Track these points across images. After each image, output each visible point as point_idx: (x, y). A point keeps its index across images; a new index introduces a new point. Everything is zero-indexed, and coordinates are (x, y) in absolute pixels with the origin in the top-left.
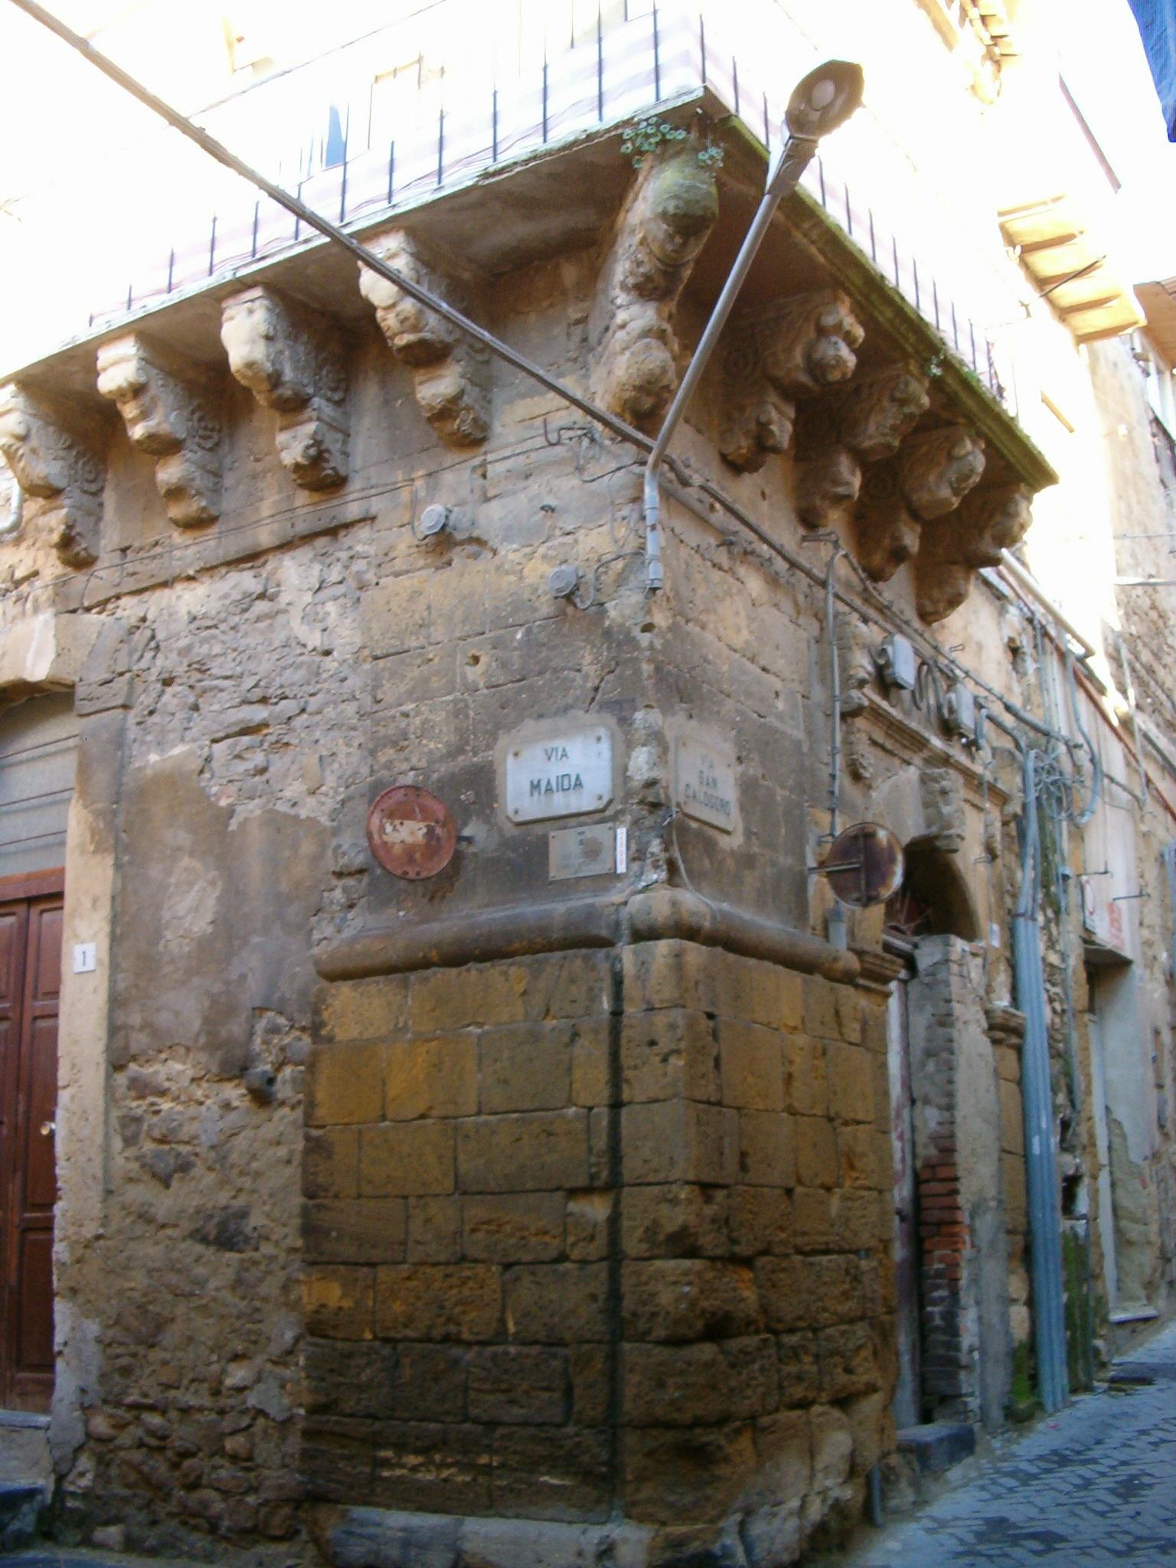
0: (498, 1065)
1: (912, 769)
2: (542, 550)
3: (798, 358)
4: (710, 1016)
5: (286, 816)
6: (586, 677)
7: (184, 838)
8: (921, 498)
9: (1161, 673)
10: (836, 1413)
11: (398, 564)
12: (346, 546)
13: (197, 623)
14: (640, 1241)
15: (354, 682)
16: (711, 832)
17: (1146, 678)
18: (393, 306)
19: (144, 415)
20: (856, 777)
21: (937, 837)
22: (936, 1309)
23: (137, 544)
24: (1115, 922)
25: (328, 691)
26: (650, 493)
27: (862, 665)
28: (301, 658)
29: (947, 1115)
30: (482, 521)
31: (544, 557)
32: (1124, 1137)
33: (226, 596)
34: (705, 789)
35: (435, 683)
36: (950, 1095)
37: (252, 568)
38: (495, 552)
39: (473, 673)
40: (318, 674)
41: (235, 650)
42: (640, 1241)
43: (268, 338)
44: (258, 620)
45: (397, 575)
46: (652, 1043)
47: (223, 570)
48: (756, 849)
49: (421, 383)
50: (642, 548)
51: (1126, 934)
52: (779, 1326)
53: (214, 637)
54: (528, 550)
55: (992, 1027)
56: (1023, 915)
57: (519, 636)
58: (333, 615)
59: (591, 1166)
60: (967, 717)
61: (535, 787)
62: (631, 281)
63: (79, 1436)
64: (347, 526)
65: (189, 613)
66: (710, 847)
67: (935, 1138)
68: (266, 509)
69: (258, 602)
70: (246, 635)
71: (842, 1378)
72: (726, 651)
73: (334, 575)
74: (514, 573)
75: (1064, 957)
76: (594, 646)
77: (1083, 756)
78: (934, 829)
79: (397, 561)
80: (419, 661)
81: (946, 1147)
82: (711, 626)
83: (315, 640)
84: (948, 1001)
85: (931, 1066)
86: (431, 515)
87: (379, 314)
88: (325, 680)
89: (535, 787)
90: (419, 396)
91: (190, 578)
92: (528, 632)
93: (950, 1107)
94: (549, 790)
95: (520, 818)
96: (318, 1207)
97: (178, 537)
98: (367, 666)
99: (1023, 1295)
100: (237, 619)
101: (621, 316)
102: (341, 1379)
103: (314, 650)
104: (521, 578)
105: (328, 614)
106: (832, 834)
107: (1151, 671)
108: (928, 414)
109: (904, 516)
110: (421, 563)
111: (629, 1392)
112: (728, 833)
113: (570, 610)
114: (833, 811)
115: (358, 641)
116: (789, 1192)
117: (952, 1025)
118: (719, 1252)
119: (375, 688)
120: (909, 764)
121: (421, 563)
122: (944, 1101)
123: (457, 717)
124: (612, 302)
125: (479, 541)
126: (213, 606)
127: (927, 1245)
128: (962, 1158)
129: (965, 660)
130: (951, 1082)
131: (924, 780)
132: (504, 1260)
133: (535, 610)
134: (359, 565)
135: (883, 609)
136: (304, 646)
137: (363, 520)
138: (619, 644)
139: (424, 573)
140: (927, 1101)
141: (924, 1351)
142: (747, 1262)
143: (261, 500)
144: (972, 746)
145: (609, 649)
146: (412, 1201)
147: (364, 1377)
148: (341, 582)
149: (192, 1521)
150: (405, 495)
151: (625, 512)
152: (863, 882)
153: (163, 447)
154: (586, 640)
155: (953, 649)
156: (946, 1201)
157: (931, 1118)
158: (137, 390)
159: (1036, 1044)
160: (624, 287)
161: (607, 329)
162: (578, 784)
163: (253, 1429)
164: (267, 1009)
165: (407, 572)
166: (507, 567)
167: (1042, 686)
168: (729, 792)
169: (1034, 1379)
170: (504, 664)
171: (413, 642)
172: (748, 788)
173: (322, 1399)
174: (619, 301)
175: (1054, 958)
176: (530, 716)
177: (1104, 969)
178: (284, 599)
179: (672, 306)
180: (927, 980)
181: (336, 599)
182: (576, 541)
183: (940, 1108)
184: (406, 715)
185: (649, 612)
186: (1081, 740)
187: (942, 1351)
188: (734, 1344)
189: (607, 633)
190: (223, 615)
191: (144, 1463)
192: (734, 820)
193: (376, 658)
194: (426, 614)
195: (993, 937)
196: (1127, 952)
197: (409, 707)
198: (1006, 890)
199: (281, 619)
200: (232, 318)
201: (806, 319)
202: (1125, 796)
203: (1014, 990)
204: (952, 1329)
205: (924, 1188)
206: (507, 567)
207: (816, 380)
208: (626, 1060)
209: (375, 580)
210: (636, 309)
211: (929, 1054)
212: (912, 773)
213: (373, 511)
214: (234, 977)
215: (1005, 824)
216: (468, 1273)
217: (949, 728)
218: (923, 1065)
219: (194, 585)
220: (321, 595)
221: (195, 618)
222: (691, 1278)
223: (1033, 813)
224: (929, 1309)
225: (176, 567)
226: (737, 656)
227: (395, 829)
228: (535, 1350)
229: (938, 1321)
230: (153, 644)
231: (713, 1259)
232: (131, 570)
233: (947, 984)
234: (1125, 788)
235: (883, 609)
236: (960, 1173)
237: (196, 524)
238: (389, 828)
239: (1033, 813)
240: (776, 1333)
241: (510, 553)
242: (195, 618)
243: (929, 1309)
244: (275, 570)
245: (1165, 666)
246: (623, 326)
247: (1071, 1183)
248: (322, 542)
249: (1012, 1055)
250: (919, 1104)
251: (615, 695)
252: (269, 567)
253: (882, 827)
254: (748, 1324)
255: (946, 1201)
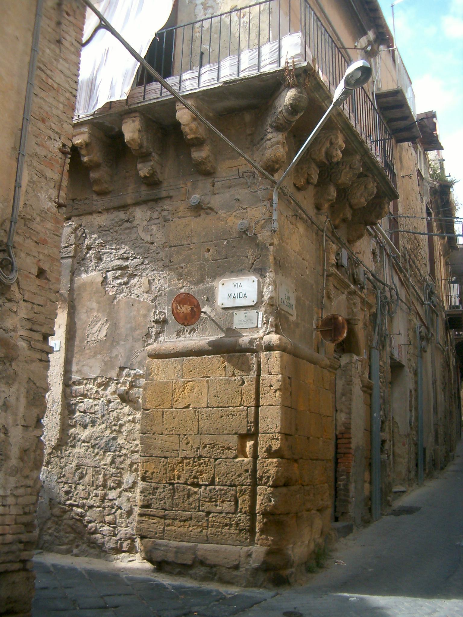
0: (215, 391)
1: (344, 295)
2: (234, 214)
3: (323, 150)
4: (289, 378)
5: (135, 300)
6: (249, 260)
7: (95, 305)
8: (354, 201)
9: (417, 262)
10: (318, 513)
11: (180, 214)
12: (160, 205)
13: (101, 229)
14: (265, 452)
15: (162, 254)
16: (287, 315)
17: (413, 264)
18: (188, 124)
19: (88, 154)
20: (329, 297)
21: (351, 319)
22: (342, 483)
23: (78, 198)
24: (400, 352)
25: (152, 257)
26: (275, 198)
27: (333, 259)
28: (142, 245)
29: (348, 415)
30: (212, 202)
31: (235, 216)
32: (398, 427)
33: (113, 220)
34: (286, 300)
35: (193, 257)
36: (350, 409)
37: (123, 210)
38: (217, 213)
39: (207, 255)
40: (148, 250)
41: (116, 239)
42: (265, 452)
43: (139, 131)
44: (126, 229)
45: (179, 218)
46: (271, 386)
47: (112, 210)
48: (299, 322)
49: (194, 152)
50: (271, 216)
51: (403, 357)
52: (304, 484)
53: (108, 234)
54: (228, 213)
55: (363, 386)
56: (374, 348)
57: (225, 243)
58: (154, 230)
59: (248, 427)
60: (362, 278)
61: (229, 296)
62: (274, 124)
63: (48, 514)
64: (161, 199)
65: (99, 225)
66: (287, 319)
67: (344, 424)
68: (130, 190)
69: (125, 223)
70: (120, 234)
71: (321, 503)
72: (293, 253)
73: (155, 215)
74: (223, 221)
75: (384, 363)
76: (252, 249)
77: (394, 293)
78: (350, 317)
79: (180, 213)
80: (187, 249)
81: (348, 427)
82: (289, 244)
83: (148, 238)
84: (351, 376)
85: (344, 399)
86: (195, 198)
87: (182, 127)
88: (151, 253)
89: (229, 296)
90: (193, 156)
91: (99, 212)
92: (228, 242)
93: (350, 413)
94: (234, 297)
95: (224, 306)
96: (147, 437)
97: (95, 197)
98: (167, 249)
99: (368, 480)
100: (117, 228)
101: (269, 136)
102: (154, 497)
103: (147, 241)
104: (226, 223)
105: (153, 229)
106: (322, 318)
107: (414, 262)
108: (362, 173)
109: (347, 205)
110: (189, 214)
111: (258, 502)
112: (292, 315)
113: (244, 236)
114: (322, 309)
115: (164, 240)
116: (308, 438)
117: (352, 385)
118: (289, 457)
119: (170, 257)
120: (343, 293)
121: (189, 214)
122: (347, 411)
123: (201, 270)
124: (266, 130)
125: (211, 209)
126: (107, 223)
127: (339, 461)
128: (353, 431)
129: (360, 257)
130: (350, 405)
131: (348, 300)
132: (216, 457)
133: (231, 235)
134: (165, 213)
135: (338, 239)
136: (144, 240)
137: (167, 197)
138: (262, 249)
139: (190, 218)
140: (341, 411)
141: (336, 497)
142: (296, 461)
143: (128, 186)
144: (362, 288)
145: (258, 250)
146: (182, 436)
147: (161, 496)
148: (158, 219)
149: (92, 545)
150: (183, 190)
151: (265, 203)
152: (333, 335)
153: (96, 166)
154: (250, 247)
155: (356, 253)
156: (347, 446)
157: (342, 417)
158: (87, 145)
159: (376, 392)
160: (271, 126)
161: (262, 139)
162: (245, 296)
163: (116, 514)
164: (126, 368)
165: (183, 217)
166: (221, 219)
167: (382, 266)
168: (293, 302)
169: (370, 510)
170: (219, 253)
171: (185, 242)
172: (298, 299)
173: (146, 503)
174: (268, 131)
175: (381, 363)
176: (228, 272)
177: (396, 367)
178: (136, 223)
179: (285, 134)
180: (343, 369)
181: (155, 224)
182: (247, 212)
183: (346, 413)
184: (182, 268)
185: (273, 239)
186: (394, 287)
187: (343, 498)
188: (293, 488)
189: (257, 245)
190: (111, 227)
191: (74, 525)
192: (294, 312)
193: (171, 247)
194: (190, 233)
195: (364, 355)
196: (404, 363)
197: (183, 265)
198: (369, 338)
199: (135, 230)
200: (126, 123)
201: (327, 139)
202: (405, 307)
203: (370, 373)
204: (347, 490)
205: (339, 441)
206: (221, 219)
207: (328, 160)
208: (261, 392)
209: (171, 219)
210: (274, 134)
211: (343, 395)
212: (344, 296)
213: (171, 194)
214: (113, 355)
215: (370, 316)
216: (202, 461)
217: (355, 282)
218: (341, 398)
219: (100, 215)
220: (149, 223)
221: (101, 227)
222: (282, 465)
223: (379, 312)
224: (339, 483)
225: (94, 208)
226: (296, 254)
227: (181, 308)
228: (226, 488)
229: (342, 487)
230: (84, 235)
231: (288, 459)
232: (76, 207)
233: (351, 371)
234: (406, 304)
235: (338, 239)
236: (352, 436)
237: (101, 194)
238: (179, 307)
239: (379, 312)
240: (303, 486)
241: (222, 213)
242: (101, 227)
243: (339, 483)
244: (132, 213)
245: (418, 260)
246: (270, 140)
247: (383, 442)
248: (150, 204)
249: (368, 397)
250: (339, 412)
251: (260, 266)
252: (130, 210)
253: (340, 316)
254: (296, 482)
255: (347, 446)
